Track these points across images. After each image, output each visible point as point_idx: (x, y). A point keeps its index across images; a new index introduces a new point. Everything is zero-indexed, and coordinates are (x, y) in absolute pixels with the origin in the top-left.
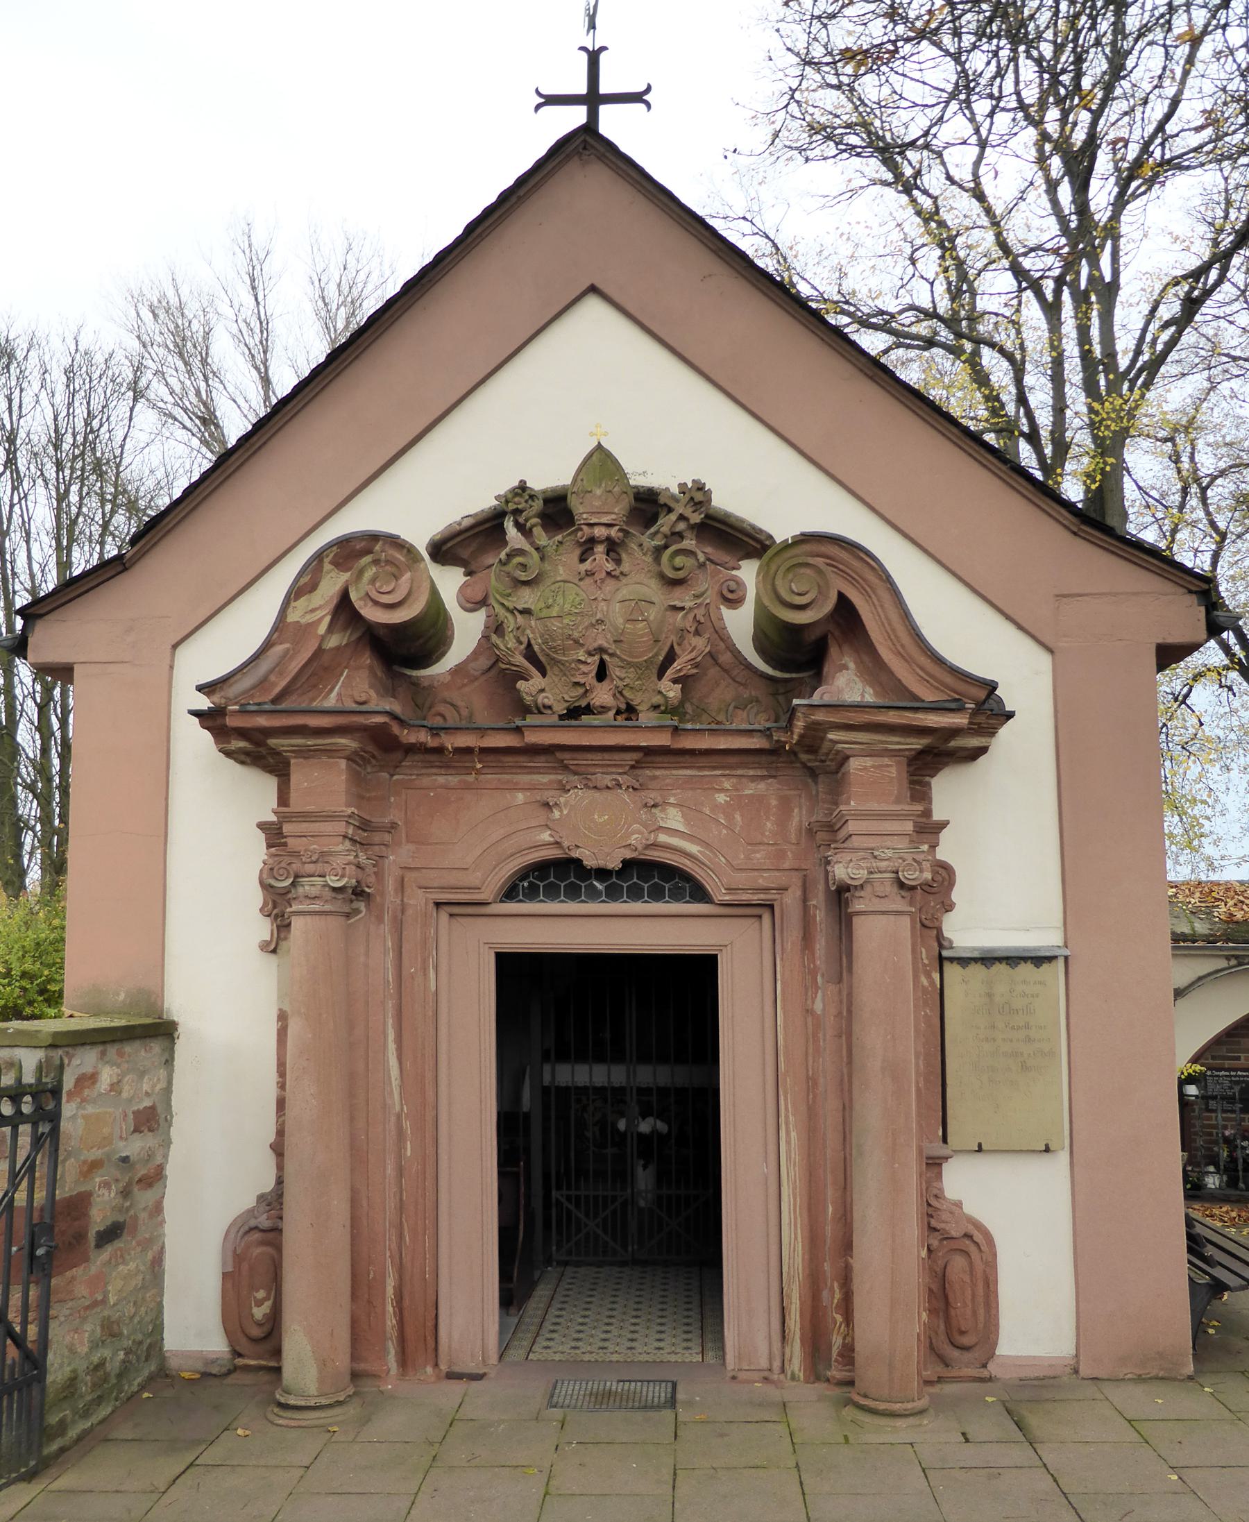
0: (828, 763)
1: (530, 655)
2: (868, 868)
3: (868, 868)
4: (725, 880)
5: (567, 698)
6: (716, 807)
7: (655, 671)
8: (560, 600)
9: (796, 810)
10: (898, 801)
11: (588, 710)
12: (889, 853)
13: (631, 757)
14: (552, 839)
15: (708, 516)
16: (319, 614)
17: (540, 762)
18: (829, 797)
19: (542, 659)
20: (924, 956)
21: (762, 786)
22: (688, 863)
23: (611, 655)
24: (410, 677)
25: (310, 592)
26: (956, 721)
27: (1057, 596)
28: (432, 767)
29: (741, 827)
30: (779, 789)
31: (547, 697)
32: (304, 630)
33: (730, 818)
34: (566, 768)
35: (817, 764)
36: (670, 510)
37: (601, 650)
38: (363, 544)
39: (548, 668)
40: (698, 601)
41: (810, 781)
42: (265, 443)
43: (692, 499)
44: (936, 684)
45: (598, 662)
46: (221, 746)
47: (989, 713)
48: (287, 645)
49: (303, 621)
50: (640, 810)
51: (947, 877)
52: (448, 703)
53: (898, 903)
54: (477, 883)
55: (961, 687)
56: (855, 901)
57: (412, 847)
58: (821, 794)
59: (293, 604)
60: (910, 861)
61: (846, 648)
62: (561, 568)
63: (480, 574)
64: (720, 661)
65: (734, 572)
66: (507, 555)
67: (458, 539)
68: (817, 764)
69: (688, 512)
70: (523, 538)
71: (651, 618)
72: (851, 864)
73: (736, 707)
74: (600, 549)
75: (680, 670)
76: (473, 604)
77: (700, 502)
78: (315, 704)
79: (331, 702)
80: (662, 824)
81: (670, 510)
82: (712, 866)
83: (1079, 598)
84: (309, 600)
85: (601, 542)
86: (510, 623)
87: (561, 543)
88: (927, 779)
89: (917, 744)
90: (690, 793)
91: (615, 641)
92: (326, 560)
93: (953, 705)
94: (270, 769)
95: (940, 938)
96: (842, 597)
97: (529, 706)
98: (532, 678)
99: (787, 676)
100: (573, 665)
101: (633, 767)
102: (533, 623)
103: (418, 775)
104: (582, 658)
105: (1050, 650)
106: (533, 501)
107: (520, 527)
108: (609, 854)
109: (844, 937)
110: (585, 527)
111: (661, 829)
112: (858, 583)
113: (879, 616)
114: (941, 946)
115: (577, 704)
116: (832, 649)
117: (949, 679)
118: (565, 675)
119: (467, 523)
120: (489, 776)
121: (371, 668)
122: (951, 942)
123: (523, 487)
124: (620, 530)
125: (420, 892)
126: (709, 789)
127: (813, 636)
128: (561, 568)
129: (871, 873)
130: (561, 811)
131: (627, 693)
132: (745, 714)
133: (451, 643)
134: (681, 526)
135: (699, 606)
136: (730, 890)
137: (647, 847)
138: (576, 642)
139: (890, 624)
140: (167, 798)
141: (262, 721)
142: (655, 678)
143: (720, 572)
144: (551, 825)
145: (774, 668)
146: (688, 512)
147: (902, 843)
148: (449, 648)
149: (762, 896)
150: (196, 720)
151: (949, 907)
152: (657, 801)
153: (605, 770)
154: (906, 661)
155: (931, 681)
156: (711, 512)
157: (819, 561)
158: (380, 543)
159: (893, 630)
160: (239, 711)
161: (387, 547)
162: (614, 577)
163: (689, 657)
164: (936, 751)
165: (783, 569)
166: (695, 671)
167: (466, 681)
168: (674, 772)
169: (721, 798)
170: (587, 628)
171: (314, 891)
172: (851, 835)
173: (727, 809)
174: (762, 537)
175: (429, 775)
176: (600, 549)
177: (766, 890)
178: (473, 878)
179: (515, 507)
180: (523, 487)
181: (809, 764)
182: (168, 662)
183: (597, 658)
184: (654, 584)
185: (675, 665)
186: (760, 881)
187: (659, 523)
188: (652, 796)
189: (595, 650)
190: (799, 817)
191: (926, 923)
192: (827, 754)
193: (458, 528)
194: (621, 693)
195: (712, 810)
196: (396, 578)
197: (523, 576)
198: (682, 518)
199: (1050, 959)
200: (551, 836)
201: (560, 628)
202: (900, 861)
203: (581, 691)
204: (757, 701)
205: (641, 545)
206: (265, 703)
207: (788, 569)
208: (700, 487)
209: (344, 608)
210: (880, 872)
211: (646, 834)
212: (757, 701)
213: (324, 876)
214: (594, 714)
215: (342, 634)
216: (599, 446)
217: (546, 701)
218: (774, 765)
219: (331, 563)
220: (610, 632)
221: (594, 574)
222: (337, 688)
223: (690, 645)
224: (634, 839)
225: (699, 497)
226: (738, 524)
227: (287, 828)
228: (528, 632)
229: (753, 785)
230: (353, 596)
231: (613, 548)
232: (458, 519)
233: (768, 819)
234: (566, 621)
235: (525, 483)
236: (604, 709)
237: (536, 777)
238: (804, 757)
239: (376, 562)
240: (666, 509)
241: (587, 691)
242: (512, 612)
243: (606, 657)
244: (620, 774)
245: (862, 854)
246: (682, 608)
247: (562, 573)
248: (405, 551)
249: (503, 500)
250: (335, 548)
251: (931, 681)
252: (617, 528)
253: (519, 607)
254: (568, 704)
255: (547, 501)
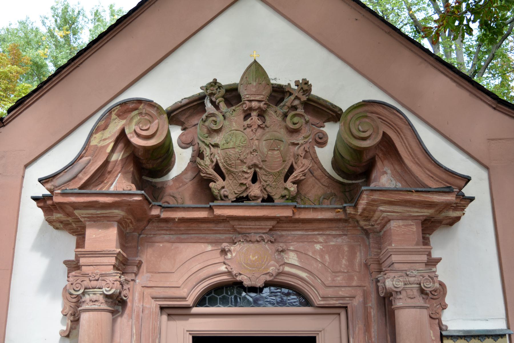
0: (376, 226)
1: (217, 168)
2: (404, 281)
3: (404, 281)
4: (321, 293)
5: (236, 192)
6: (315, 251)
7: (283, 177)
8: (234, 139)
9: (358, 254)
10: (417, 244)
11: (247, 198)
12: (415, 273)
13: (270, 224)
14: (226, 270)
15: (309, 100)
16: (108, 142)
17: (221, 227)
18: (376, 245)
19: (224, 171)
20: (432, 335)
21: (339, 240)
22: (300, 283)
23: (261, 168)
24: (151, 182)
25: (104, 129)
26: (446, 198)
27: (489, 139)
28: (162, 230)
29: (329, 263)
30: (349, 242)
31: (225, 191)
32: (100, 149)
33: (322, 256)
34: (235, 230)
35: (370, 227)
36: (291, 94)
37: (255, 165)
38: (133, 105)
39: (226, 176)
40: (306, 140)
41: (365, 237)
42: (82, 63)
43: (302, 88)
44: (437, 179)
45: (253, 173)
46: (47, 217)
47: (462, 197)
48: (89, 158)
49: (99, 145)
50: (275, 253)
51: (442, 290)
52: (171, 196)
53: (419, 301)
54: (184, 295)
55: (451, 180)
56: (397, 301)
57: (149, 275)
58: (371, 244)
59: (94, 136)
60: (427, 277)
61: (386, 162)
62: (234, 123)
63: (190, 129)
64: (314, 175)
65: (322, 129)
66: (206, 117)
67: (180, 110)
68: (370, 227)
69: (300, 95)
70: (214, 109)
71: (282, 149)
72: (395, 279)
73: (324, 198)
74: (254, 114)
75: (297, 177)
76: (184, 145)
77: (307, 90)
78: (104, 190)
79: (112, 189)
80: (286, 261)
81: (291, 94)
82: (314, 285)
83: (500, 141)
84: (103, 134)
85: (255, 110)
86: (207, 152)
87: (234, 110)
88: (427, 235)
89: (427, 212)
90: (301, 244)
91: (262, 161)
92: (113, 113)
93: (447, 190)
94: (73, 232)
95: (440, 324)
96: (384, 134)
97: (217, 196)
98: (218, 181)
99: (350, 182)
100: (240, 174)
101: (271, 230)
102: (219, 151)
103: (154, 234)
104: (245, 170)
105: (486, 168)
106: (220, 89)
107: (213, 103)
108: (257, 278)
109: (388, 324)
110: (247, 102)
111: (285, 264)
112: (393, 126)
113: (405, 143)
114: (441, 329)
115: (241, 195)
116: (378, 163)
117: (444, 176)
118: (235, 179)
119: (184, 102)
120: (193, 235)
121: (133, 174)
122: (447, 327)
123: (215, 82)
124: (265, 104)
125: (153, 300)
126: (311, 242)
127: (367, 157)
128: (234, 123)
129: (405, 284)
130: (232, 254)
131: (268, 189)
132: (329, 201)
133: (174, 165)
134: (296, 102)
135: (306, 142)
136: (324, 298)
137: (279, 274)
138: (242, 161)
139: (411, 148)
140: (14, 249)
141: (73, 199)
142: (283, 181)
143: (314, 128)
144: (226, 262)
145: (343, 178)
146: (300, 95)
147: (422, 267)
148: (173, 167)
149: (341, 302)
150: (34, 203)
151: (444, 307)
152: (284, 248)
153: (256, 231)
154: (420, 166)
155: (435, 177)
156: (310, 97)
157: (374, 116)
158: (143, 105)
159: (413, 150)
160: (60, 194)
161: (146, 107)
162: (261, 128)
163: (301, 170)
164: (433, 219)
165: (354, 119)
166: (303, 177)
167: (181, 185)
168: (293, 233)
169: (318, 247)
170: (248, 154)
171: (94, 297)
172: (393, 263)
173: (322, 253)
174: (337, 110)
175: (160, 234)
176: (254, 114)
177: (343, 298)
178: (182, 292)
179: (211, 92)
180: (215, 82)
181: (365, 228)
182: (21, 174)
183: (253, 170)
184: (283, 132)
185: (294, 174)
186: (340, 293)
187: (285, 101)
188: (281, 246)
189: (252, 165)
190: (359, 258)
191: (433, 316)
192: (376, 220)
193: (180, 104)
194: (265, 189)
195: (313, 253)
196: (150, 122)
197: (215, 127)
198: (297, 98)
199: (502, 336)
200: (226, 268)
201: (233, 154)
202: (421, 277)
203: (244, 188)
204: (335, 195)
205: (276, 112)
206: (75, 189)
207: (357, 119)
208: (306, 82)
209: (122, 137)
210: (411, 284)
211: (278, 267)
212: (335, 195)
213: (101, 289)
214: (250, 200)
215: (119, 153)
216: (255, 61)
217: (225, 193)
218: (346, 229)
219: (116, 114)
220: (260, 156)
221: (251, 126)
222: (114, 183)
223: (302, 163)
224: (272, 270)
225: (305, 87)
226: (324, 103)
227: (82, 261)
228: (216, 156)
229: (335, 240)
230: (127, 131)
231: (262, 114)
232: (180, 100)
233: (343, 258)
234: (237, 150)
235: (216, 80)
236: (256, 198)
237: (218, 236)
238: (362, 223)
239: (140, 114)
240: (288, 94)
241: (247, 188)
242: (208, 146)
243: (258, 170)
244: (264, 233)
245: (400, 274)
246: (298, 144)
247: (235, 126)
248: (156, 109)
249: (205, 88)
250: (118, 107)
251: (435, 177)
252: (264, 102)
253: (213, 143)
254: (237, 195)
255: (227, 91)
